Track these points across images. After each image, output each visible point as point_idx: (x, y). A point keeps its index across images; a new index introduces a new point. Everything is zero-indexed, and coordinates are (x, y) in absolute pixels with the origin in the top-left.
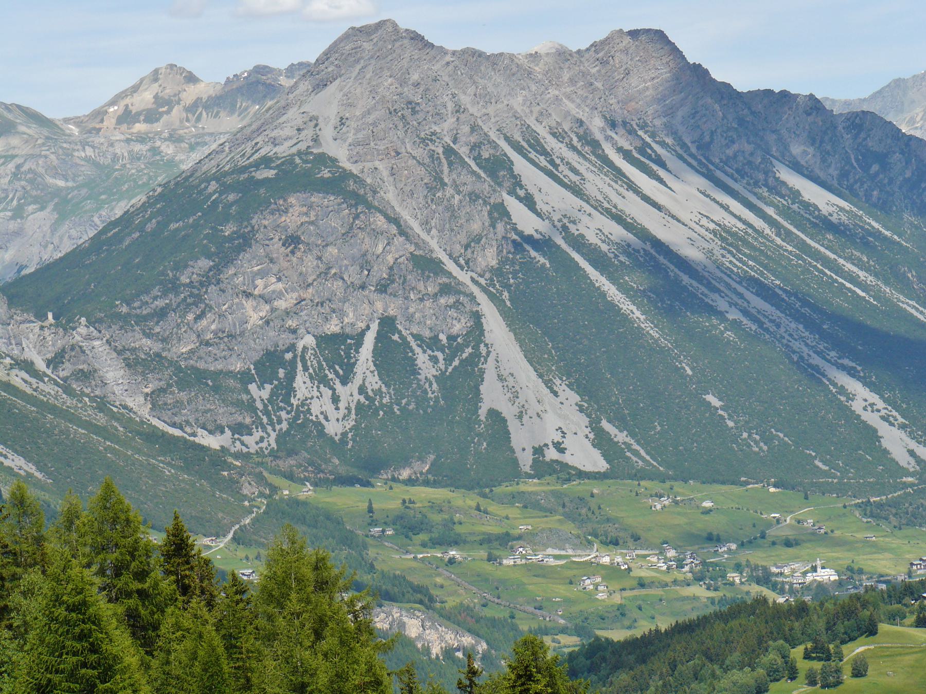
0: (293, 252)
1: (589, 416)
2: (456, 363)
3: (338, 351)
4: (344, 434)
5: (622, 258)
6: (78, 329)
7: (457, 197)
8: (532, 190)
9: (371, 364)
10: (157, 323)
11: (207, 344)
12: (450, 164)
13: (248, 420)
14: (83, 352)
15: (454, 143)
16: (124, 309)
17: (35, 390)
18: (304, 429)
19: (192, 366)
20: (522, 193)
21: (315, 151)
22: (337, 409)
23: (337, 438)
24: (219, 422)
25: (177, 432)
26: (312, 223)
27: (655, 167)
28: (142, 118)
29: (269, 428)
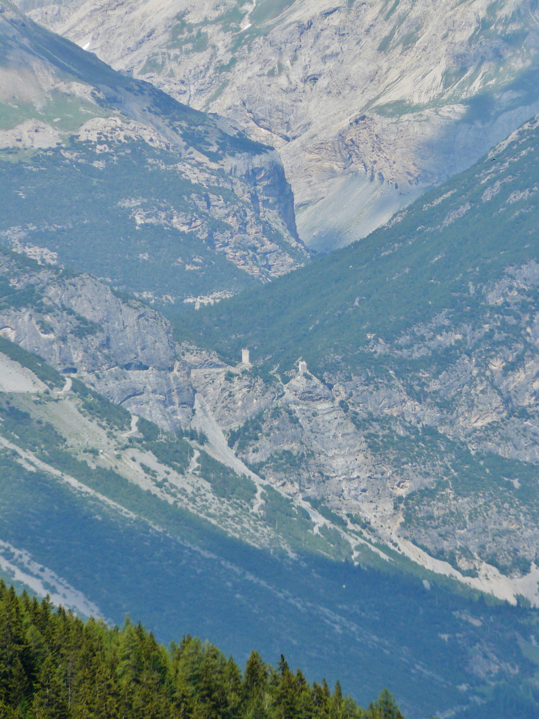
6: (293, 382)
10: (435, 376)
11: (524, 414)
14: (295, 421)
16: (380, 348)
17: (159, 485)
19: (490, 454)
24: (521, 554)
25: (442, 568)
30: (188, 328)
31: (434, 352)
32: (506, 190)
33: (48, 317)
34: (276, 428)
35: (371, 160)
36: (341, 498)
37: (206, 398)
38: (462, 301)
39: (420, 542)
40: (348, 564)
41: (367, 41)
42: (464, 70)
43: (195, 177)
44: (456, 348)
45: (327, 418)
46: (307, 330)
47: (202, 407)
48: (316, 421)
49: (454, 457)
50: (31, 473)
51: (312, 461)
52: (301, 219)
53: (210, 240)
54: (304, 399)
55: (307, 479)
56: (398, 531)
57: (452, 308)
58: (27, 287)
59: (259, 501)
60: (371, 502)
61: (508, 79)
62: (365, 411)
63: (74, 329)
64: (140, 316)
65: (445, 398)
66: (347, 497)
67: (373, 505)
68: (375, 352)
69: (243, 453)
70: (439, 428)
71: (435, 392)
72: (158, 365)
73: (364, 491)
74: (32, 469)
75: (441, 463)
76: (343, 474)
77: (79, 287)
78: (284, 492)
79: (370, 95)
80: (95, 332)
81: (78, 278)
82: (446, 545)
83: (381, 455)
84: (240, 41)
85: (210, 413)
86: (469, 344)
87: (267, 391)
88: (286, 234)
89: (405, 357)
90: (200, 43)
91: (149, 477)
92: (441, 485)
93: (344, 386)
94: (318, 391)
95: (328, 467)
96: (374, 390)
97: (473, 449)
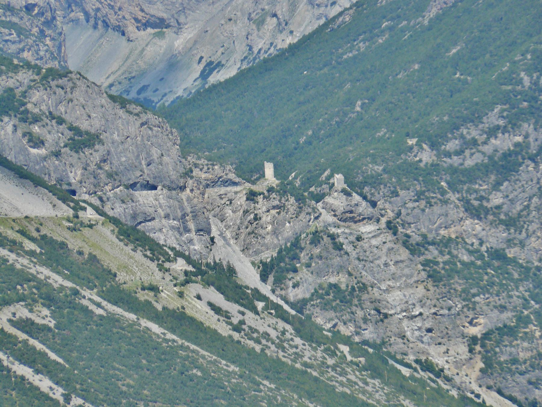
10: (497, 186)
14: (339, 247)
16: (426, 156)
17: (237, 328)
31: (491, 158)
33: (36, 128)
34: (317, 257)
35: (94, 7)
36: (405, 341)
37: (224, 223)
38: (516, 96)
39: (507, 393)
44: (517, 154)
45: (374, 242)
46: (298, 143)
47: (221, 235)
48: (362, 247)
49: (531, 286)
50: (101, 317)
51: (365, 297)
54: (345, 221)
55: (363, 319)
56: (478, 379)
57: (505, 104)
58: (5, 92)
60: (440, 344)
62: (419, 233)
63: (67, 141)
64: (142, 124)
65: (510, 214)
66: (411, 339)
67: (443, 348)
68: (420, 161)
69: (281, 289)
70: (507, 251)
71: (498, 207)
72: (168, 183)
73: (429, 330)
74: (100, 311)
75: (517, 294)
76: (403, 311)
77: (69, 89)
80: (94, 145)
81: (66, 79)
83: (444, 285)
85: (232, 242)
86: (532, 147)
87: (300, 212)
89: (456, 165)
91: (222, 319)
92: (523, 321)
93: (390, 202)
94: (360, 209)
95: (384, 303)
96: (426, 206)
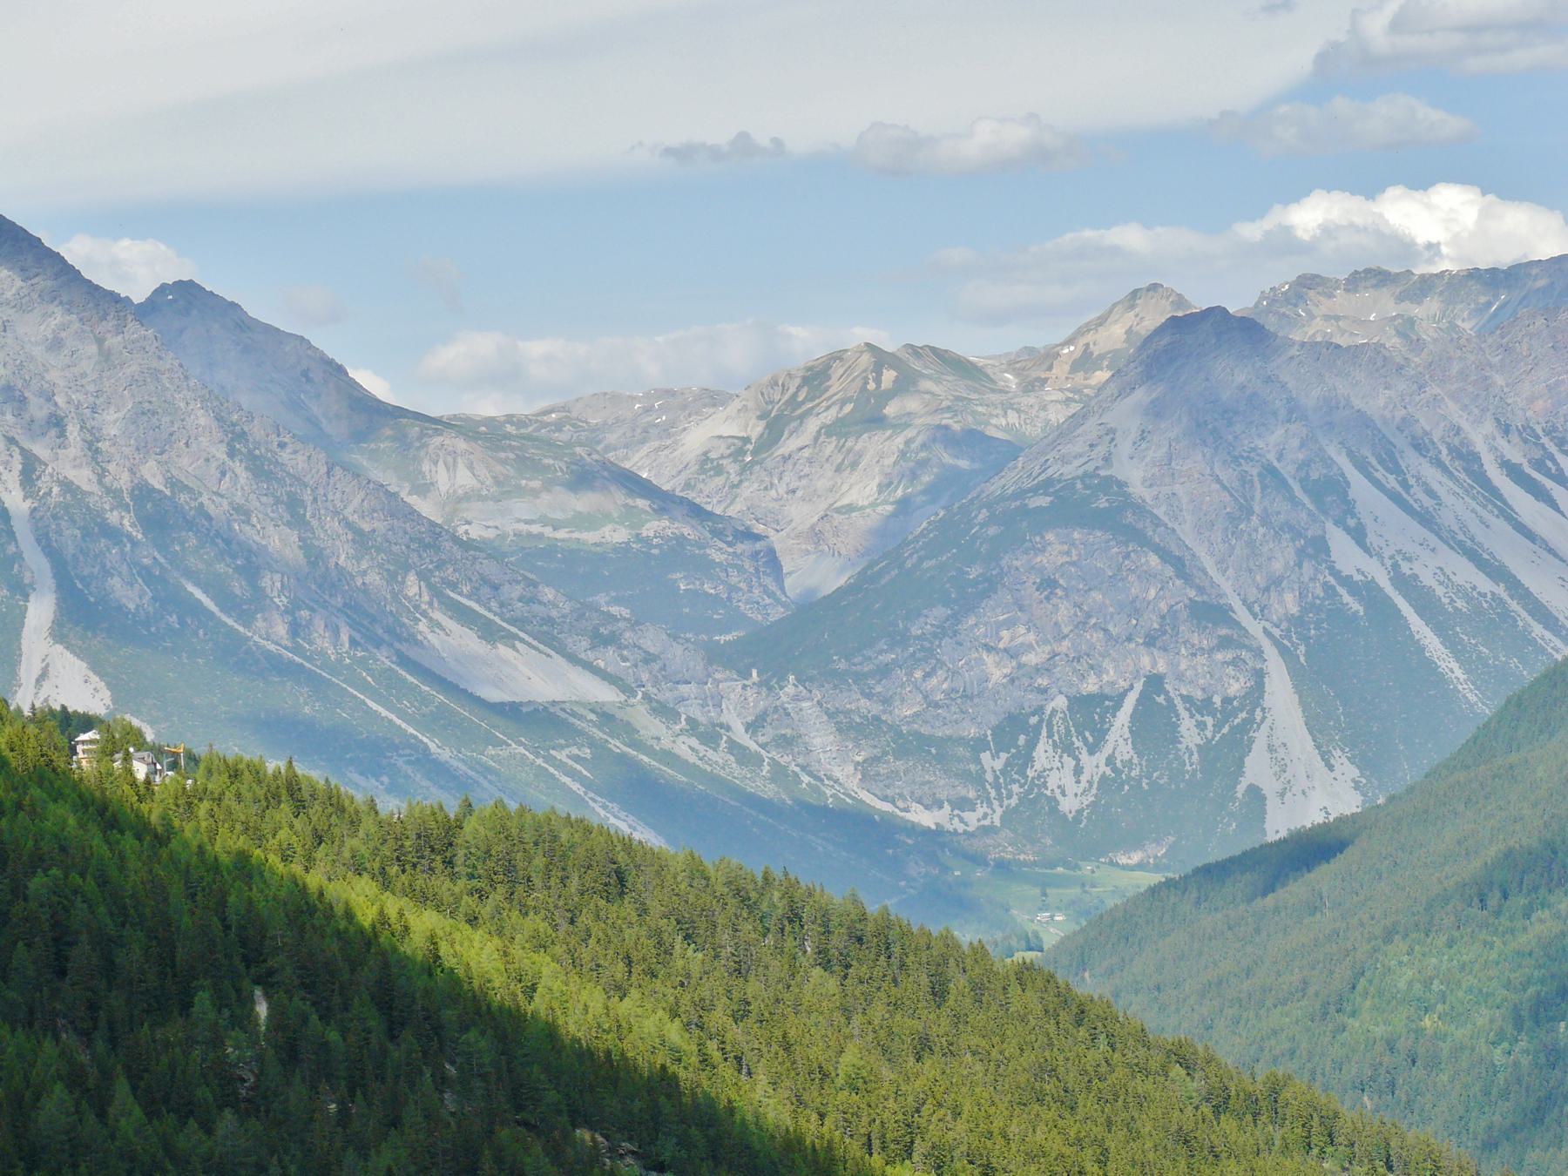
0: (1047, 598)
1: (1363, 794)
2: (1225, 730)
3: (1090, 714)
4: (1080, 812)
5: (1460, 604)
7: (1262, 530)
8: (1367, 521)
9: (1126, 730)
11: (937, 705)
12: (1264, 488)
13: (972, 794)
15: (1279, 460)
16: (842, 665)
18: (1036, 806)
20: (1351, 523)
21: (1102, 473)
22: (1078, 782)
23: (1070, 816)
25: (886, 807)
26: (1073, 564)
27: (1549, 484)
28: (1106, 363)
29: (996, 803)
30: (716, 656)
32: (921, 560)
40: (826, 806)
41: (827, 466)
42: (891, 483)
43: (718, 557)
52: (788, 582)
53: (729, 598)
59: (766, 768)
61: (920, 488)
78: (782, 761)
79: (830, 501)
82: (889, 792)
84: (745, 469)
88: (778, 593)
90: (719, 470)
92: (885, 753)
97: (904, 729)
